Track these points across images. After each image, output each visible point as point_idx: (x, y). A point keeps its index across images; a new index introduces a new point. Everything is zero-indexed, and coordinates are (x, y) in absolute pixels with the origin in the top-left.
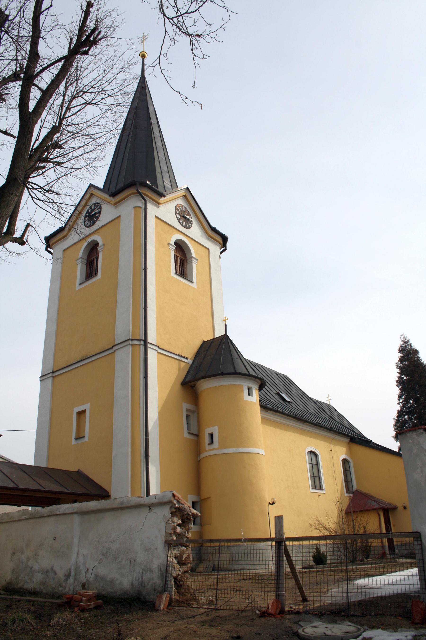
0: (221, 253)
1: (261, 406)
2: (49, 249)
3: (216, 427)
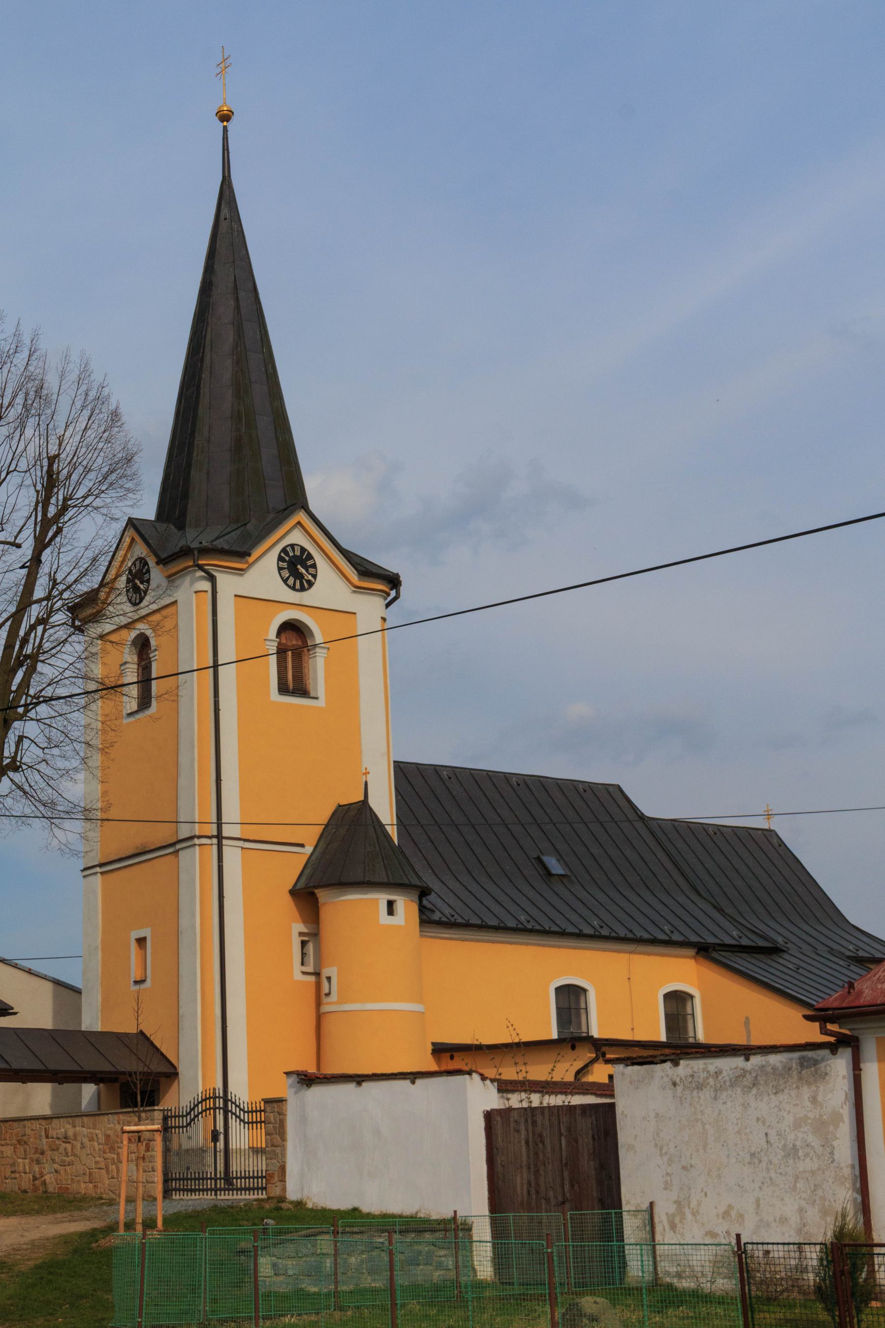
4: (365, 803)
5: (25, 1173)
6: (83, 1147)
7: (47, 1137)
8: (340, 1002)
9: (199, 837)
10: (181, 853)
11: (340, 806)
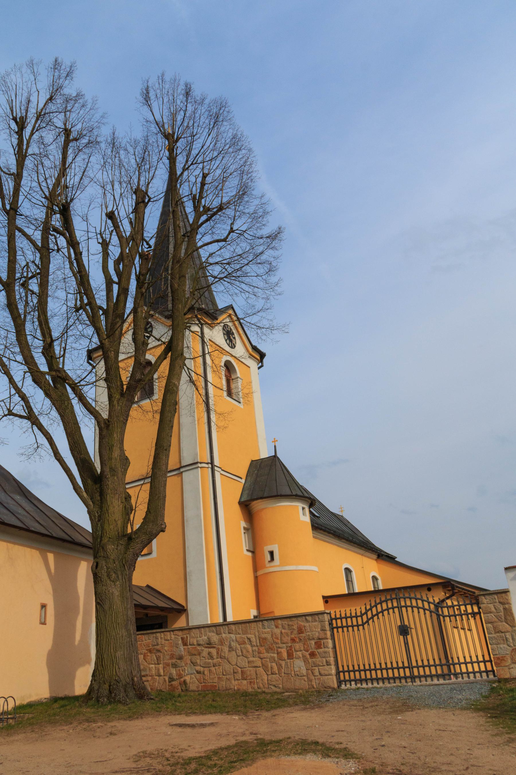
0: (259, 368)
1: (313, 526)
2: (90, 361)
3: (276, 546)
4: (275, 456)
5: (160, 676)
6: (230, 648)
7: (185, 644)
8: (281, 565)
9: (201, 463)
10: (184, 474)
11: (252, 461)
